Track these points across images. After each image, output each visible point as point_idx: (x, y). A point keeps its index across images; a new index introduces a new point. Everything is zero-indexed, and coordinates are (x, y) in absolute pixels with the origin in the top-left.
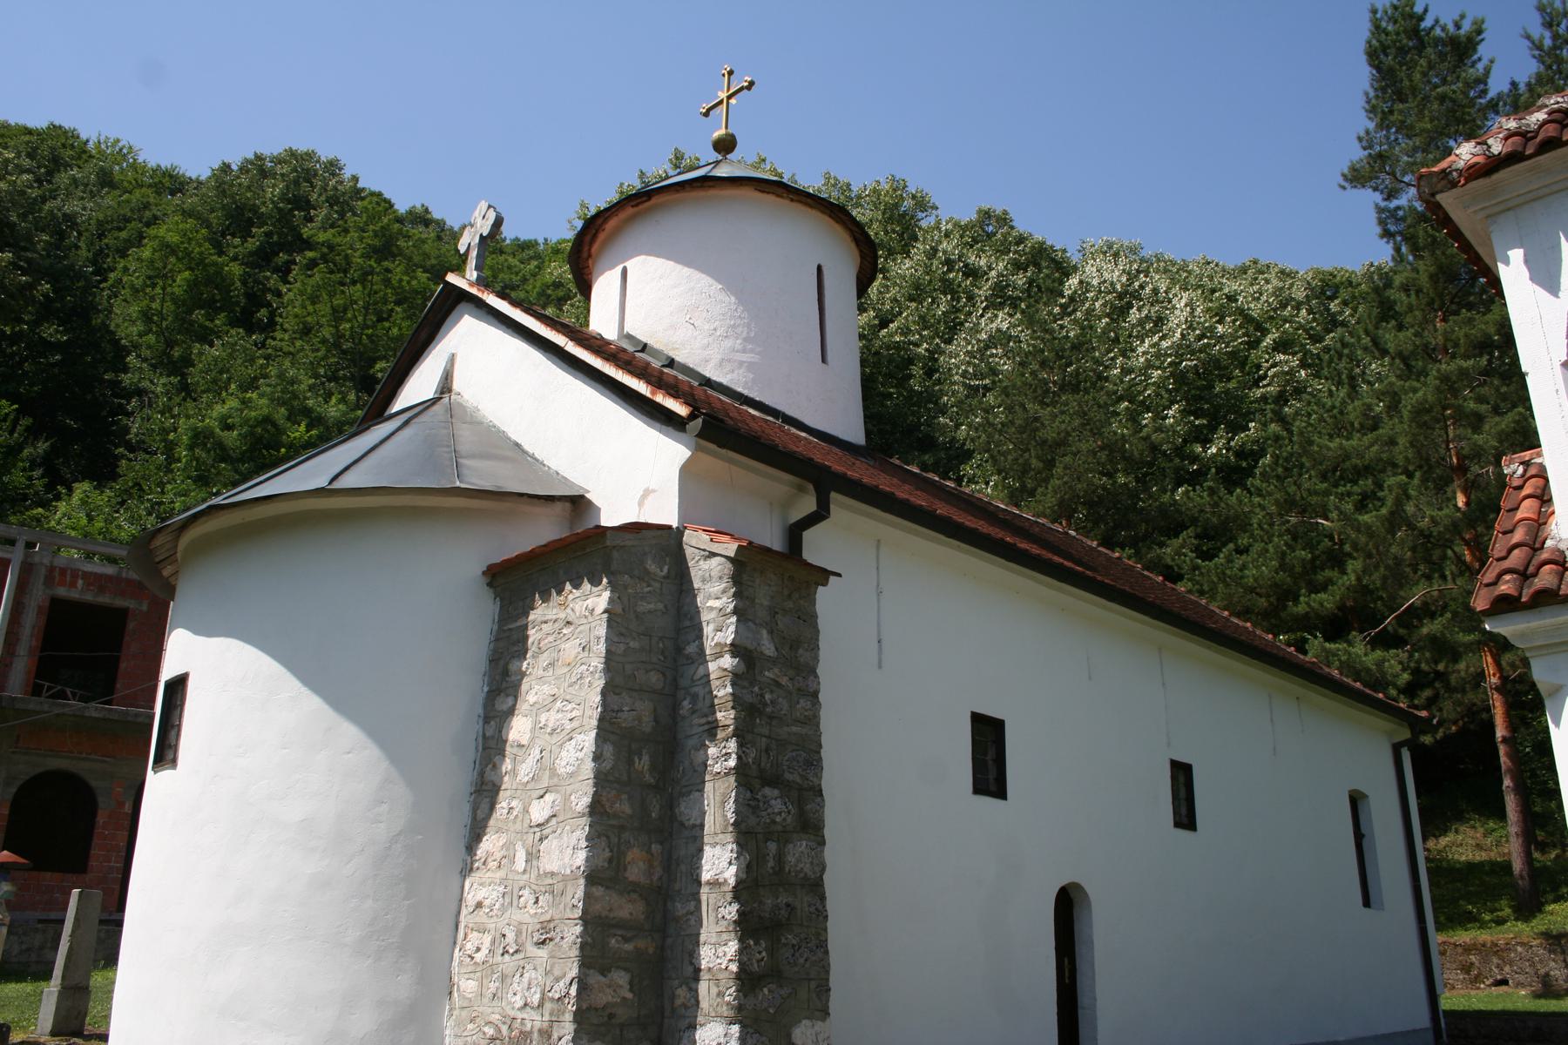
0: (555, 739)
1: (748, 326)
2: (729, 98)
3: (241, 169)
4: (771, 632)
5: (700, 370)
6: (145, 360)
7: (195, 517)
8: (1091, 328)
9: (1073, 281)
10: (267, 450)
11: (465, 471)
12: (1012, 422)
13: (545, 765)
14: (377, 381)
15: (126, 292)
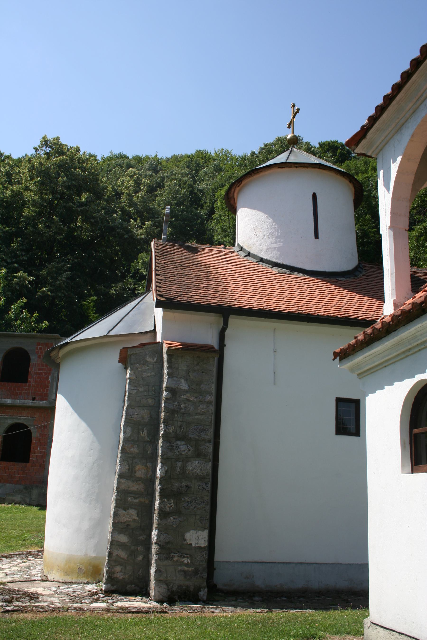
1: (278, 231)
3: (259, 153)
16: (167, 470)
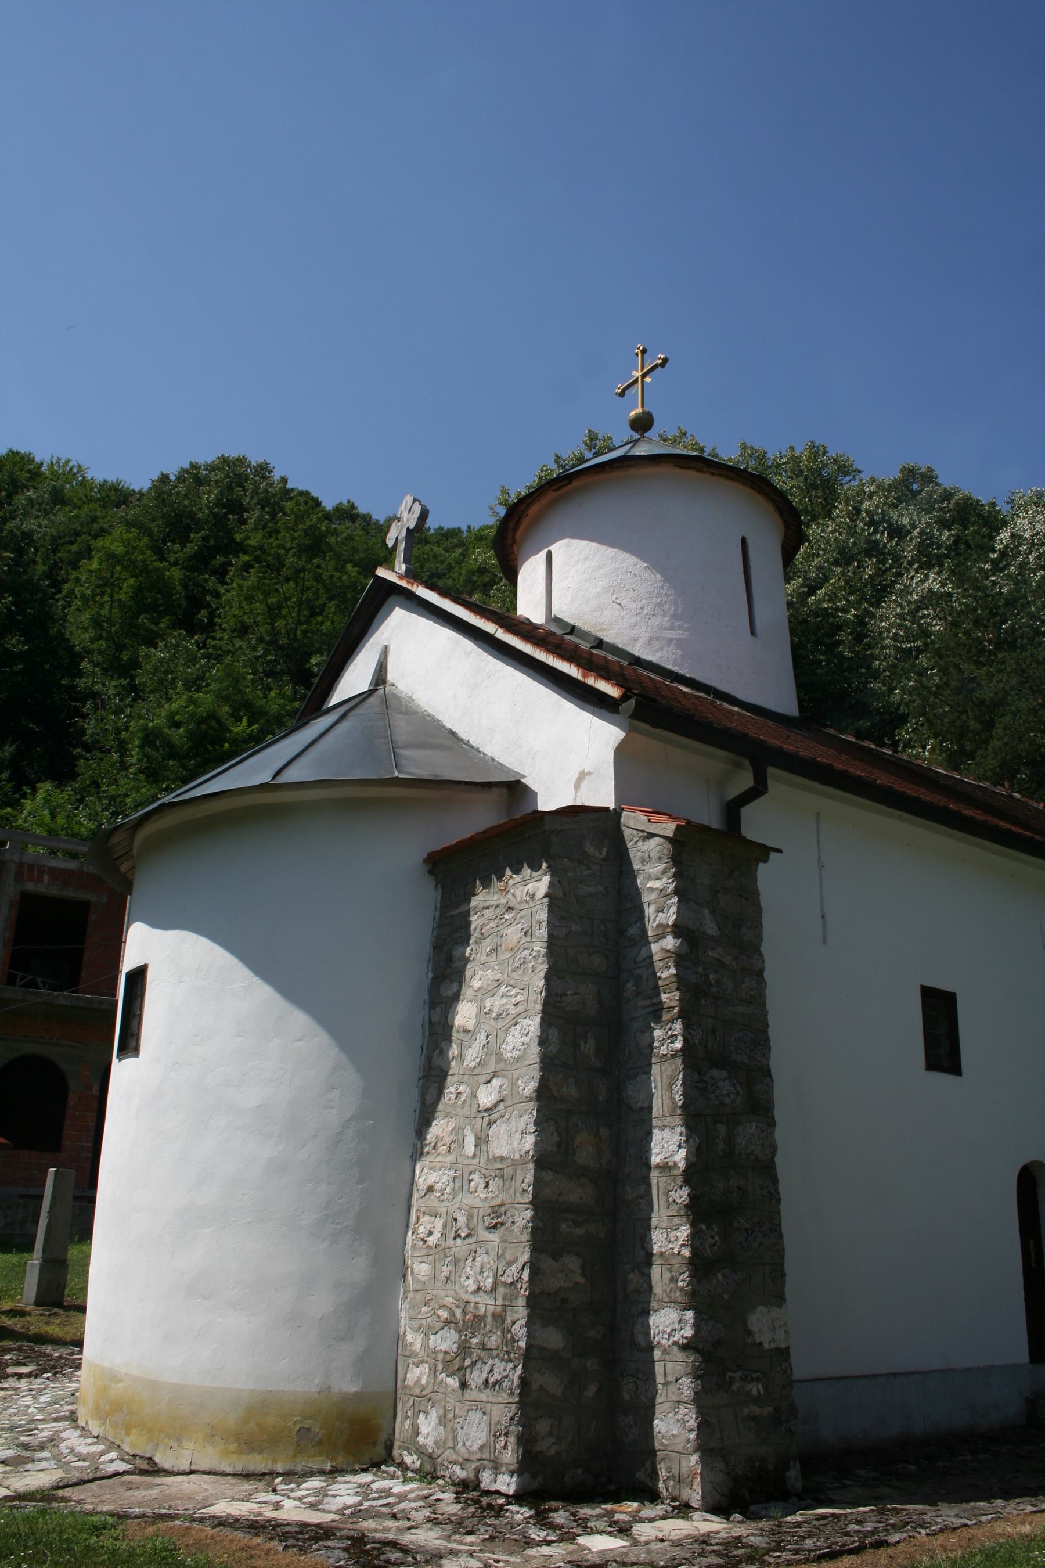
0: (500, 1023)
1: (675, 603)
2: (644, 376)
3: (178, 478)
4: (713, 911)
5: (629, 649)
6: (97, 665)
7: (148, 815)
8: (1025, 582)
9: (1005, 535)
10: (212, 748)
11: (403, 762)
12: (947, 684)
13: (492, 1050)
14: (314, 675)
15: (78, 603)
16: (700, 1145)
